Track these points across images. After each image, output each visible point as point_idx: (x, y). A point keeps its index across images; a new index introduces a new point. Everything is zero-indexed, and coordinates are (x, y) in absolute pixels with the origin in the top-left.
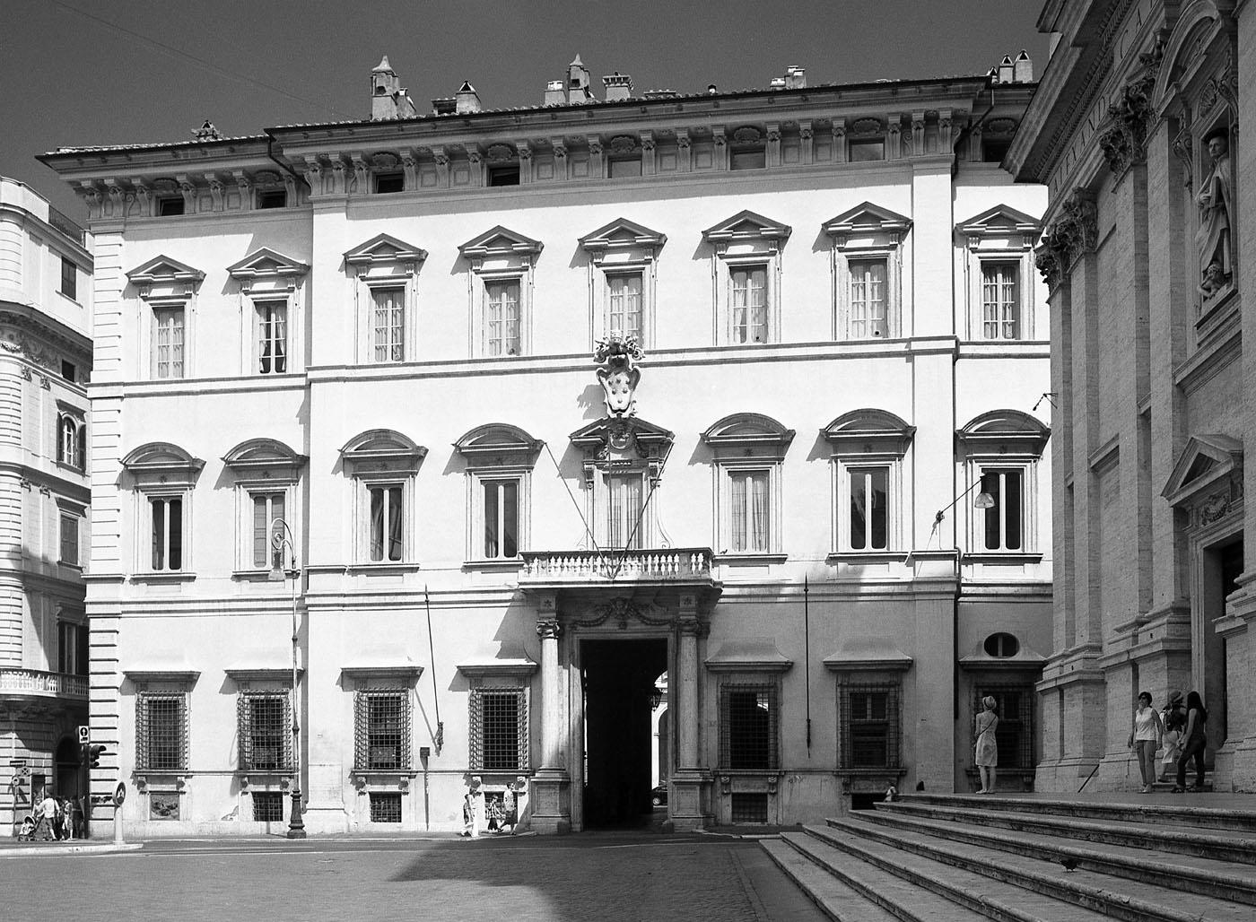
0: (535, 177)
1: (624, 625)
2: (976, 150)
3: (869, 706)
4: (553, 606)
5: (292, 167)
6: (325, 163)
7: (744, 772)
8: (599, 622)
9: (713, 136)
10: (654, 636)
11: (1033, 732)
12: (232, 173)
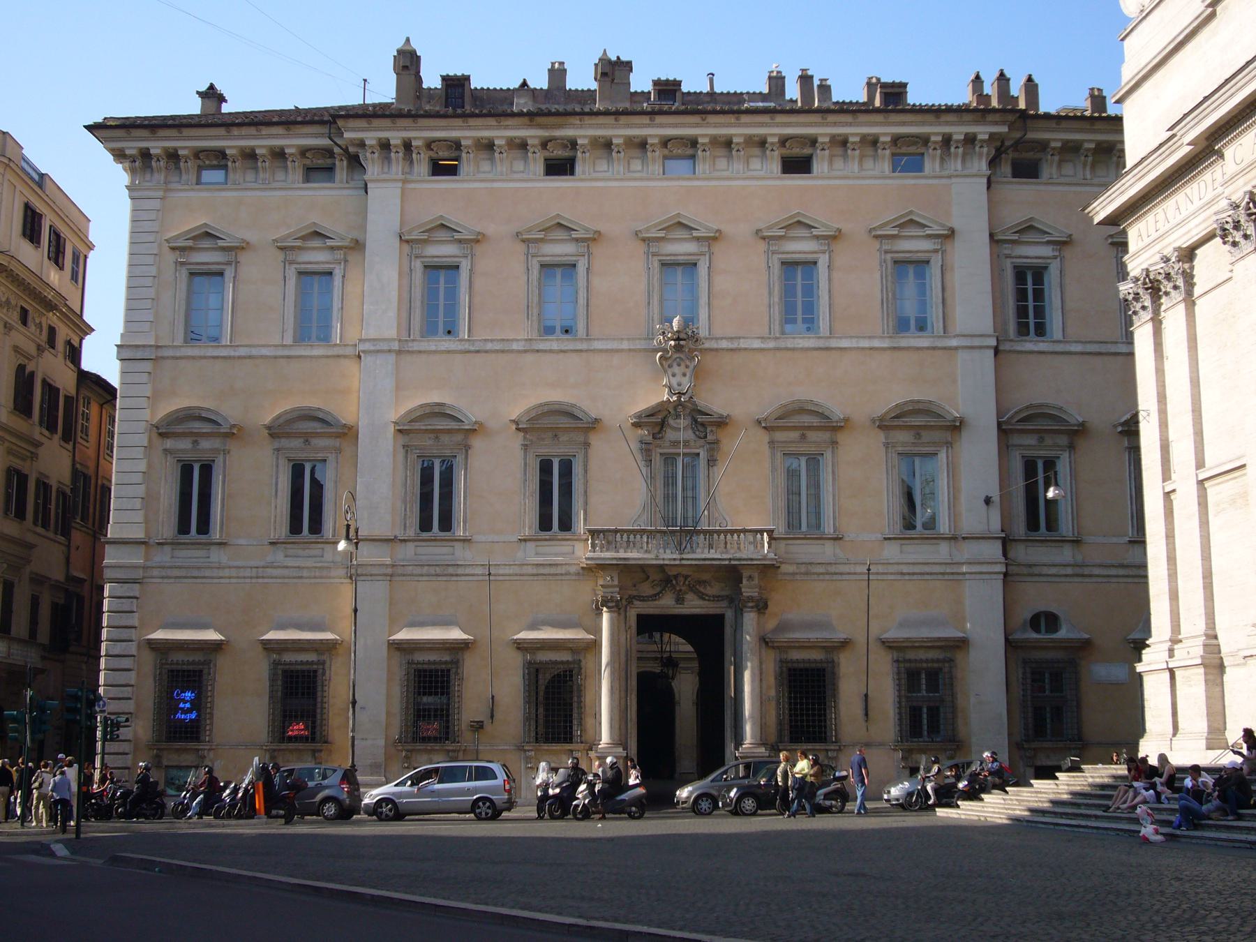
0: (592, 171)
1: (680, 600)
2: (1006, 169)
3: (924, 681)
4: (616, 582)
5: (347, 148)
6: (385, 146)
7: (178, 745)
8: (655, 597)
9: (412, 146)
10: (712, 611)
11: (1079, 706)
12: (177, 151)
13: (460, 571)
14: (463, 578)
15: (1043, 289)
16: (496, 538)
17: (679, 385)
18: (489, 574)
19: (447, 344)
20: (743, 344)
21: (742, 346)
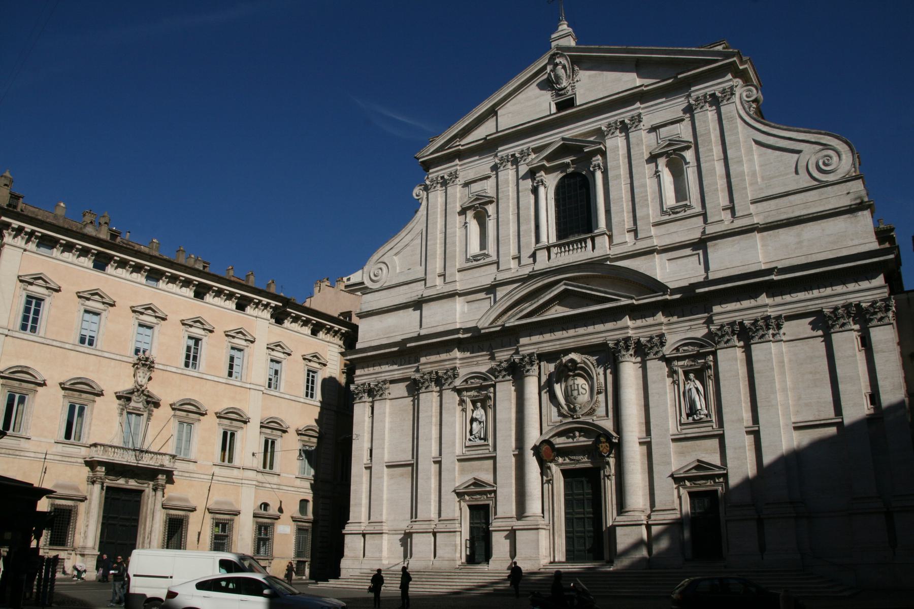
13: (22, 454)
14: (23, 458)
15: (39, 310)
16: (43, 440)
17: (141, 382)
18: (45, 459)
19: (32, 337)
20: (169, 369)
21: (168, 369)
